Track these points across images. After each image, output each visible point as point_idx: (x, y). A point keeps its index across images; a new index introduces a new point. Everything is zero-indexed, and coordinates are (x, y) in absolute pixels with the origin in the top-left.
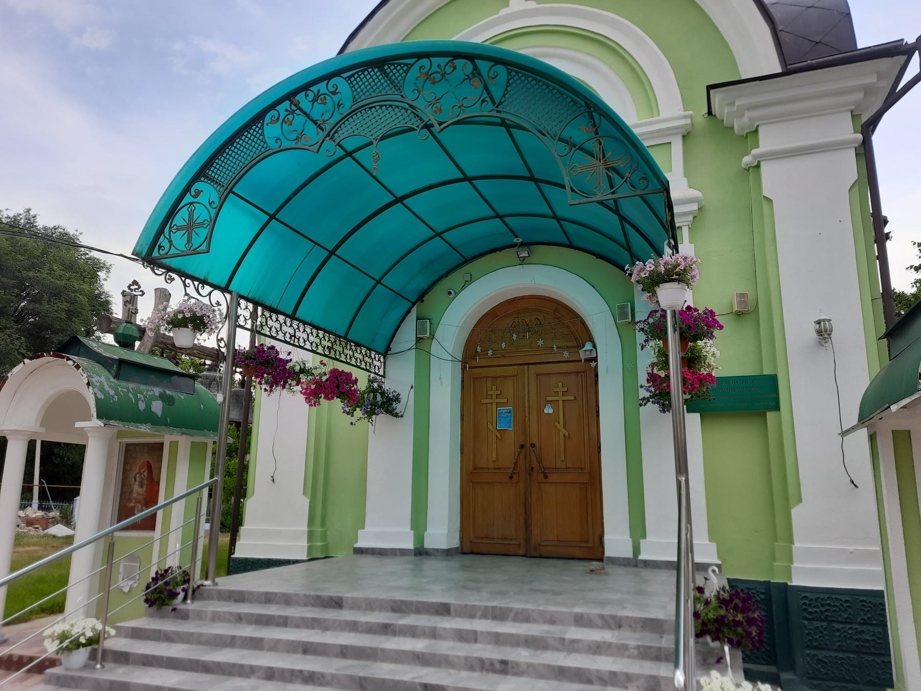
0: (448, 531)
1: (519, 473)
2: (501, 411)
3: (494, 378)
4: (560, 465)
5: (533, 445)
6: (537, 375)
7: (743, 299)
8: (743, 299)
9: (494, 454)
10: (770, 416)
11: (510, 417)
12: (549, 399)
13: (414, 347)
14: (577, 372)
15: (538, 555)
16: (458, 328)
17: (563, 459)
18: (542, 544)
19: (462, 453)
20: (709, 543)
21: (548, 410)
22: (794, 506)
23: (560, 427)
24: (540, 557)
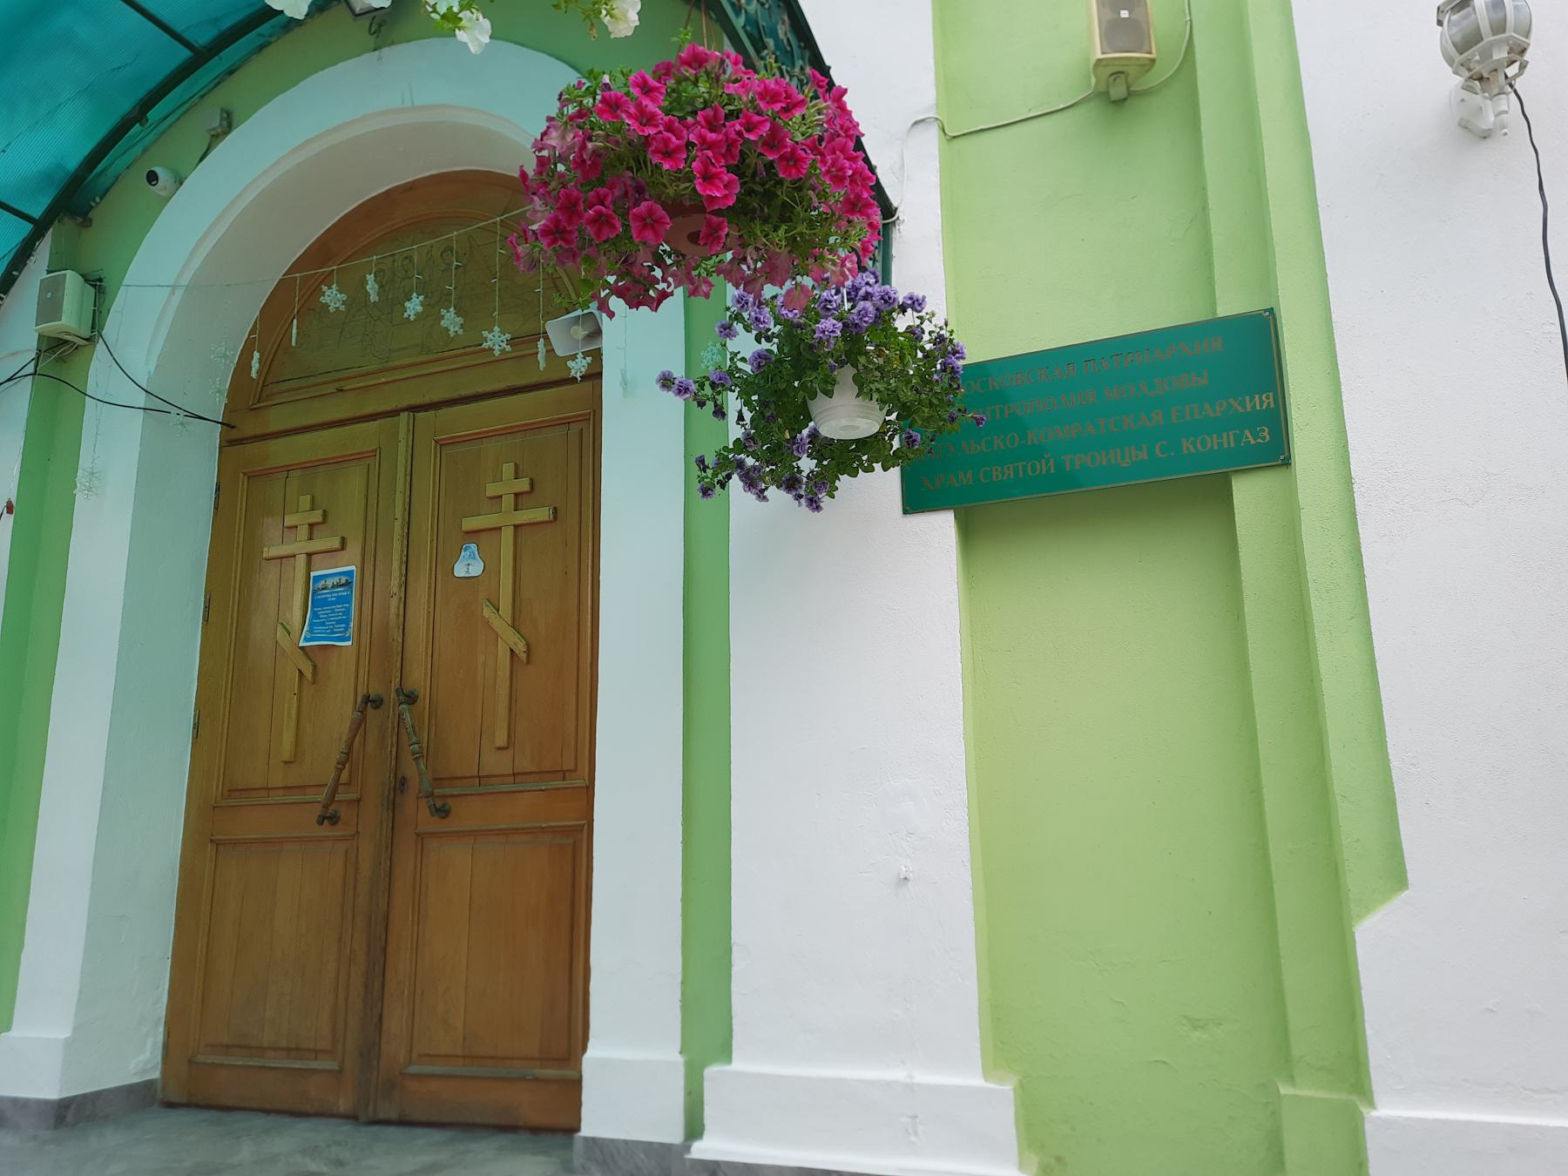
0: (77, 1029)
1: (359, 801)
2: (321, 584)
3: (309, 466)
4: (496, 763)
5: (411, 699)
6: (441, 444)
7: (1124, 14)
8: (1124, 14)
9: (288, 737)
10: (1248, 493)
11: (347, 600)
12: (470, 524)
13: (30, 369)
14: (567, 422)
15: (394, 1116)
16: (179, 293)
17: (501, 740)
18: (413, 1069)
19: (196, 737)
20: (978, 1081)
21: (469, 565)
22: (1368, 909)
23: (500, 622)
24: (403, 1122)
